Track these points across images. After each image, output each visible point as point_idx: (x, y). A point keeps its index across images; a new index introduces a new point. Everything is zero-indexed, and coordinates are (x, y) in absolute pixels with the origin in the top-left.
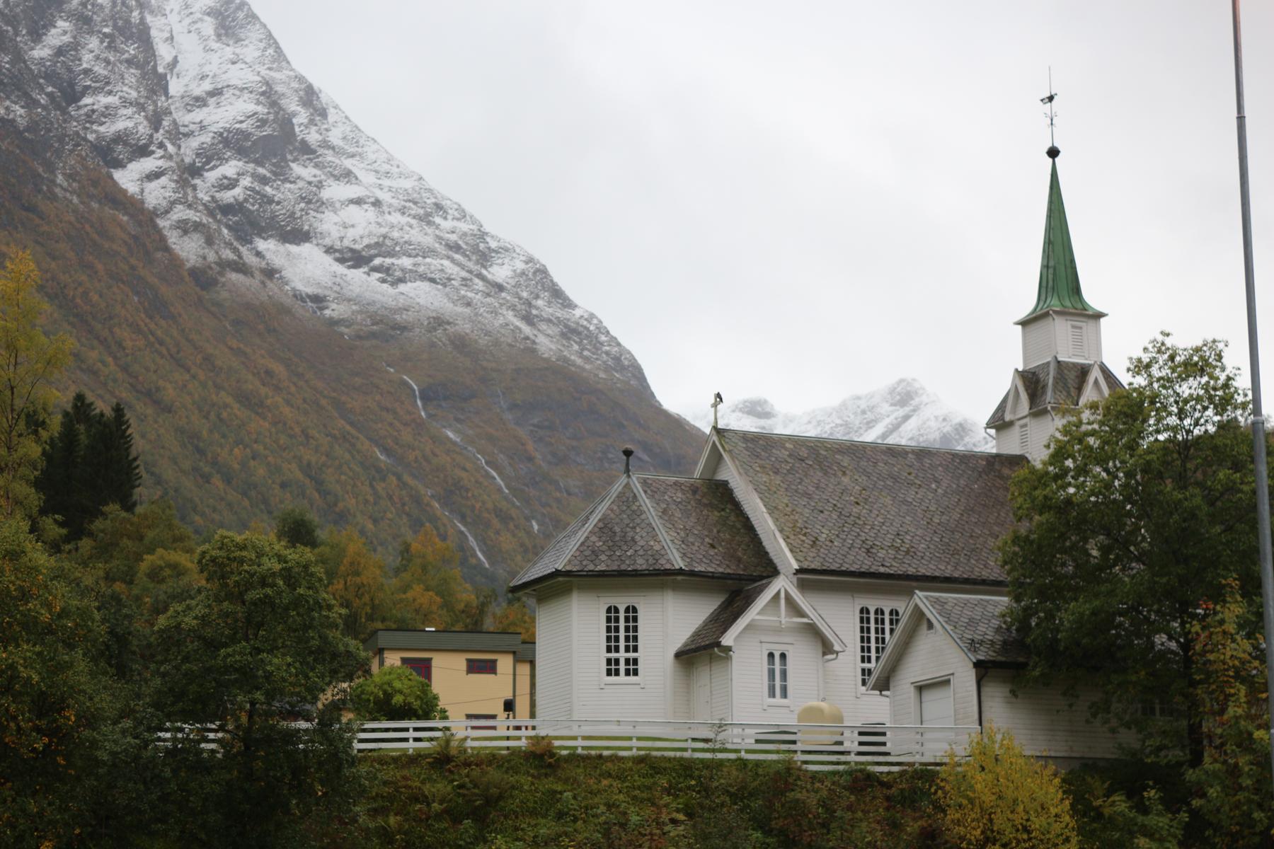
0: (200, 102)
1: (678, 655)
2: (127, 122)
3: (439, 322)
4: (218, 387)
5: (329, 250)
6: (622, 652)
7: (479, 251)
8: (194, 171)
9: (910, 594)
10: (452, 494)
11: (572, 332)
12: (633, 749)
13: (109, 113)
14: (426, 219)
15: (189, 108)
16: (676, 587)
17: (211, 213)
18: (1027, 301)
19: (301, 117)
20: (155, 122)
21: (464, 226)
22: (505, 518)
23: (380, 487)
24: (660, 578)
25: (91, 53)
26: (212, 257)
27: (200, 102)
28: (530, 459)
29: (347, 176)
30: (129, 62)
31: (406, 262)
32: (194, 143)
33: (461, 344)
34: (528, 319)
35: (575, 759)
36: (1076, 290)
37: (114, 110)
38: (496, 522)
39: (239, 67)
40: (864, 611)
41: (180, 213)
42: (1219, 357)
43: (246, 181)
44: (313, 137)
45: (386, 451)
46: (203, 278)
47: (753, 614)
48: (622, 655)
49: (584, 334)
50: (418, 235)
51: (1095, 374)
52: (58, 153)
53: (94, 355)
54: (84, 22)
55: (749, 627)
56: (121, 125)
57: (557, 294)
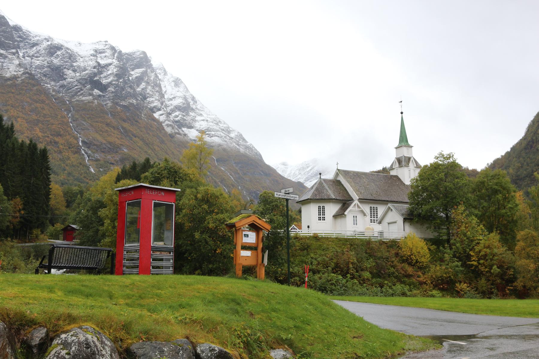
0: (171, 99)
1: (333, 216)
2: (156, 104)
3: (220, 145)
4: (175, 158)
5: (197, 130)
6: (322, 216)
7: (228, 131)
8: (170, 114)
9: (387, 204)
10: (223, 181)
11: (247, 147)
12: (334, 236)
13: (153, 102)
14: (217, 124)
15: (169, 101)
16: (333, 202)
17: (173, 123)
18: (397, 143)
19: (192, 103)
20: (162, 104)
21: (225, 126)
22: (233, 186)
23: (208, 179)
24: (329, 200)
25: (149, 90)
26: (173, 131)
27: (171, 99)
28: (239, 174)
29: (201, 115)
30: (157, 91)
31: (213, 133)
32: (170, 108)
33: (224, 150)
34: (238, 145)
35: (322, 238)
36: (407, 141)
37: (154, 101)
38: (232, 187)
39: (179, 92)
40: (371, 207)
41: (167, 122)
42: (453, 155)
43: (180, 116)
44: (194, 107)
45: (209, 172)
46: (172, 136)
47: (351, 208)
48: (322, 216)
49: (249, 148)
50: (215, 127)
51: (412, 159)
52: (142, 110)
53: (150, 152)
54: (148, 83)
55: (350, 211)
56: (155, 104)
57: (244, 140)
